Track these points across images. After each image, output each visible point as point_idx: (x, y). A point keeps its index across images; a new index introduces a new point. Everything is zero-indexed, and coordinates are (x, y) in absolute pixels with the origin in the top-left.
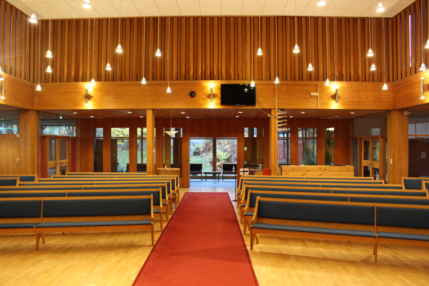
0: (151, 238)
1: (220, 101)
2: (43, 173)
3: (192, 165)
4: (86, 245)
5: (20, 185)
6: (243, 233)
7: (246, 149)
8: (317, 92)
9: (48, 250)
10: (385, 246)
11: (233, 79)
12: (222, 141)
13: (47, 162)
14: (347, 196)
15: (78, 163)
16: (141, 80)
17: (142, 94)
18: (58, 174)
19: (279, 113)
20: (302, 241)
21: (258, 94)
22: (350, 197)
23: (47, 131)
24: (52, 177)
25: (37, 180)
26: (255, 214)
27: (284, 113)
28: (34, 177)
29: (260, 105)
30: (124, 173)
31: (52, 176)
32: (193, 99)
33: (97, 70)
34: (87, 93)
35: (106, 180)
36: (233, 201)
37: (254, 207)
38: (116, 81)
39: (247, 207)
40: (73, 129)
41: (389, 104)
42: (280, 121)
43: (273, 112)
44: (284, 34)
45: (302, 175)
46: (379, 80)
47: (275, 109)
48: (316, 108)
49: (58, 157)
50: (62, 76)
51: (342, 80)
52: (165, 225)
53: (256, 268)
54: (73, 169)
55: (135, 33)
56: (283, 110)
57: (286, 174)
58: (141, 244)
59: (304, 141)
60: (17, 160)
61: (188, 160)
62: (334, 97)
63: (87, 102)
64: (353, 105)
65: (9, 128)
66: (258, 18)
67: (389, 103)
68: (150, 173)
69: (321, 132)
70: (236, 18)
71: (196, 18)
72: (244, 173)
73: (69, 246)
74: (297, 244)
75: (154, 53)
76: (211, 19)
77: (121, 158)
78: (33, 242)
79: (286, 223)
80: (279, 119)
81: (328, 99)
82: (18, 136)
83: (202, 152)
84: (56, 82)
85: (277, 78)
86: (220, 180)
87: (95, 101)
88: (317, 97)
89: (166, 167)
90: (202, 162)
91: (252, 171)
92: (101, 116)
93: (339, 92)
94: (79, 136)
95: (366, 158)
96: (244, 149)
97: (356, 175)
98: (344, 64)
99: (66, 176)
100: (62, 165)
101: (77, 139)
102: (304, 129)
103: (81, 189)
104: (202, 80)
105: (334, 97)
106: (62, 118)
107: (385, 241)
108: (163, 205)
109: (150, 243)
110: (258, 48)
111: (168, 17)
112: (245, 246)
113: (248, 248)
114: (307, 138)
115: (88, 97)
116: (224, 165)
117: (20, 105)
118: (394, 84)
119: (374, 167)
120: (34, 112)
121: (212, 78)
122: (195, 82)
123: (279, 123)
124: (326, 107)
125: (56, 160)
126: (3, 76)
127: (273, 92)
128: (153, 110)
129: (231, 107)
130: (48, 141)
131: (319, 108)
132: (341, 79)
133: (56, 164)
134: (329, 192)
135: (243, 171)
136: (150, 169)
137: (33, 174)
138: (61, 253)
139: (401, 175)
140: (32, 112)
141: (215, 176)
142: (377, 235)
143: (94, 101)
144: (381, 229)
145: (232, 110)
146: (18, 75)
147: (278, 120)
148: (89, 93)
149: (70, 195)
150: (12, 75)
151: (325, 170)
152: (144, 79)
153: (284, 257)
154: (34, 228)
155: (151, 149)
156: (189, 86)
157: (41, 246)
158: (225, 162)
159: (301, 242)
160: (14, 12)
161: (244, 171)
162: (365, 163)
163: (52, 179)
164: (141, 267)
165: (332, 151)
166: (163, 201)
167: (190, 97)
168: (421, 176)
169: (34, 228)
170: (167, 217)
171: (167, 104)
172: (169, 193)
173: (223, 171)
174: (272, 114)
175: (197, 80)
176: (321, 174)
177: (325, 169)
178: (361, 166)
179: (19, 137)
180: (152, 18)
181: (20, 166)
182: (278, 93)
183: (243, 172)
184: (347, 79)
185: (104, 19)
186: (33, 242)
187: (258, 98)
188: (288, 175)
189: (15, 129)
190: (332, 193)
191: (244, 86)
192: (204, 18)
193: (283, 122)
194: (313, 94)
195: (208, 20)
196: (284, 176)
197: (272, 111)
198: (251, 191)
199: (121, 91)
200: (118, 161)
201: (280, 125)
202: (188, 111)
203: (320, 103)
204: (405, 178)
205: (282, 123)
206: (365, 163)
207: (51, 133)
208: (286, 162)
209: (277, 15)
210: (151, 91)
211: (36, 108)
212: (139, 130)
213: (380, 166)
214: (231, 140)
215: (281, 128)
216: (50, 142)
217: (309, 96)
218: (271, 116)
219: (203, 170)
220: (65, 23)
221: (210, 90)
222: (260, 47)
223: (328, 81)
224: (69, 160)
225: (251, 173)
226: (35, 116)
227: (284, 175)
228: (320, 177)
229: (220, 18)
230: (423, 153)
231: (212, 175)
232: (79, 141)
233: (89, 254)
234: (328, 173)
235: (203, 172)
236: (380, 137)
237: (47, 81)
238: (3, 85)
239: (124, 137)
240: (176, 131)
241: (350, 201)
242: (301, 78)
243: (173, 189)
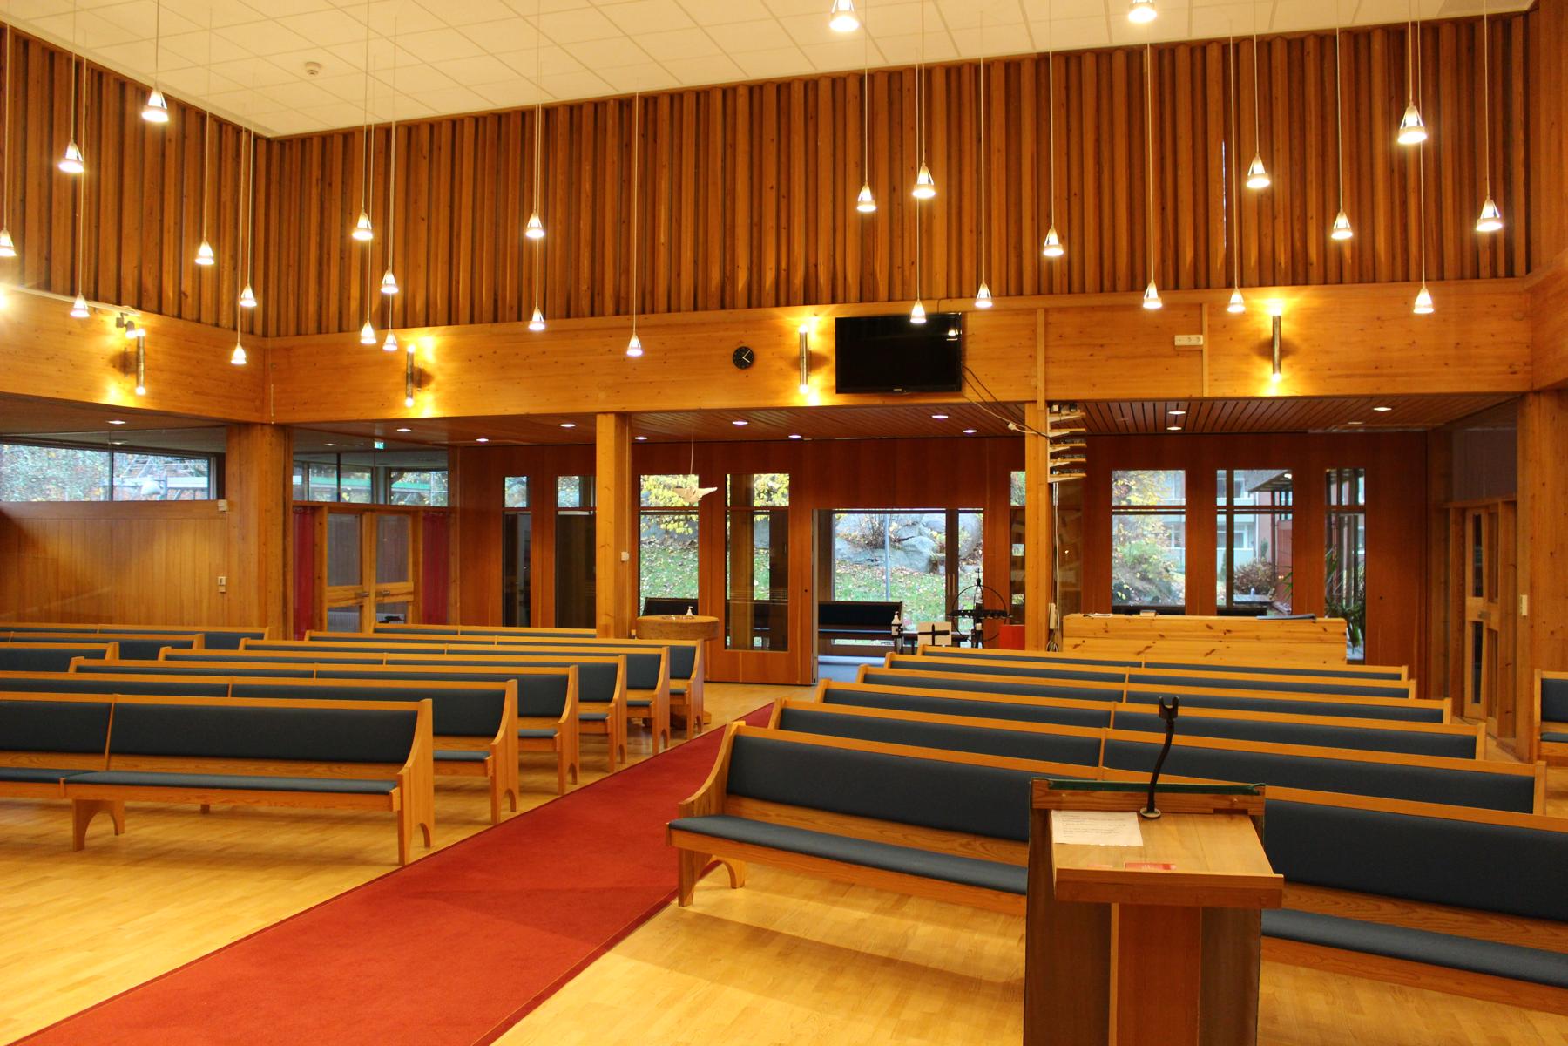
1: (833, 382)
8: (1201, 332)
11: (886, 299)
13: (321, 589)
15: (454, 594)
16: (974, 295)
17: (582, 364)
19: (1056, 418)
27: (1077, 414)
32: (742, 374)
34: (412, 366)
35: (442, 652)
41: (1511, 370)
42: (1060, 448)
45: (1139, 653)
46: (1468, 272)
51: (1306, 283)
55: (561, 156)
57: (1076, 646)
60: (219, 583)
63: (411, 396)
64: (1347, 376)
66: (977, 68)
67: (1510, 367)
68: (606, 633)
76: (810, 86)
77: (675, 578)
79: (807, 820)
80: (1055, 441)
81: (1247, 356)
85: (984, 291)
87: (437, 390)
88: (1201, 351)
94: (458, 505)
98: (1312, 218)
101: (453, 515)
103: (309, 675)
104: (777, 304)
106: (385, 445)
110: (862, 185)
114: (1290, 513)
115: (418, 378)
118: (1526, 287)
120: (268, 430)
122: (756, 313)
123: (1054, 456)
124: (1235, 391)
125: (361, 583)
127: (1030, 339)
133: (362, 596)
135: (930, 630)
136: (608, 618)
140: (262, 429)
143: (437, 390)
145: (1213, 404)
147: (1051, 443)
149: (240, 692)
150: (166, 315)
151: (1228, 634)
152: (537, 315)
154: (62, 783)
156: (728, 329)
167: (735, 368)
169: (62, 783)
171: (659, 393)
174: (1026, 424)
175: (760, 306)
176: (1213, 651)
177: (1229, 631)
178: (1463, 622)
179: (225, 508)
180: (615, 100)
181: (229, 600)
182: (1046, 342)
183: (930, 636)
184: (653, 309)
185: (443, 120)
190: (234, 695)
193: (1073, 451)
194: (1182, 340)
199: (517, 354)
201: (1060, 462)
203: (1211, 374)
204: (1551, 675)
205: (1067, 456)
209: (869, 67)
210: (610, 351)
211: (272, 416)
215: (1063, 473)
218: (1024, 429)
221: (1270, 325)
222: (867, 183)
224: (415, 585)
226: (271, 444)
227: (1070, 648)
232: (458, 520)
236: (1500, 504)
238: (142, 352)
240: (702, 485)
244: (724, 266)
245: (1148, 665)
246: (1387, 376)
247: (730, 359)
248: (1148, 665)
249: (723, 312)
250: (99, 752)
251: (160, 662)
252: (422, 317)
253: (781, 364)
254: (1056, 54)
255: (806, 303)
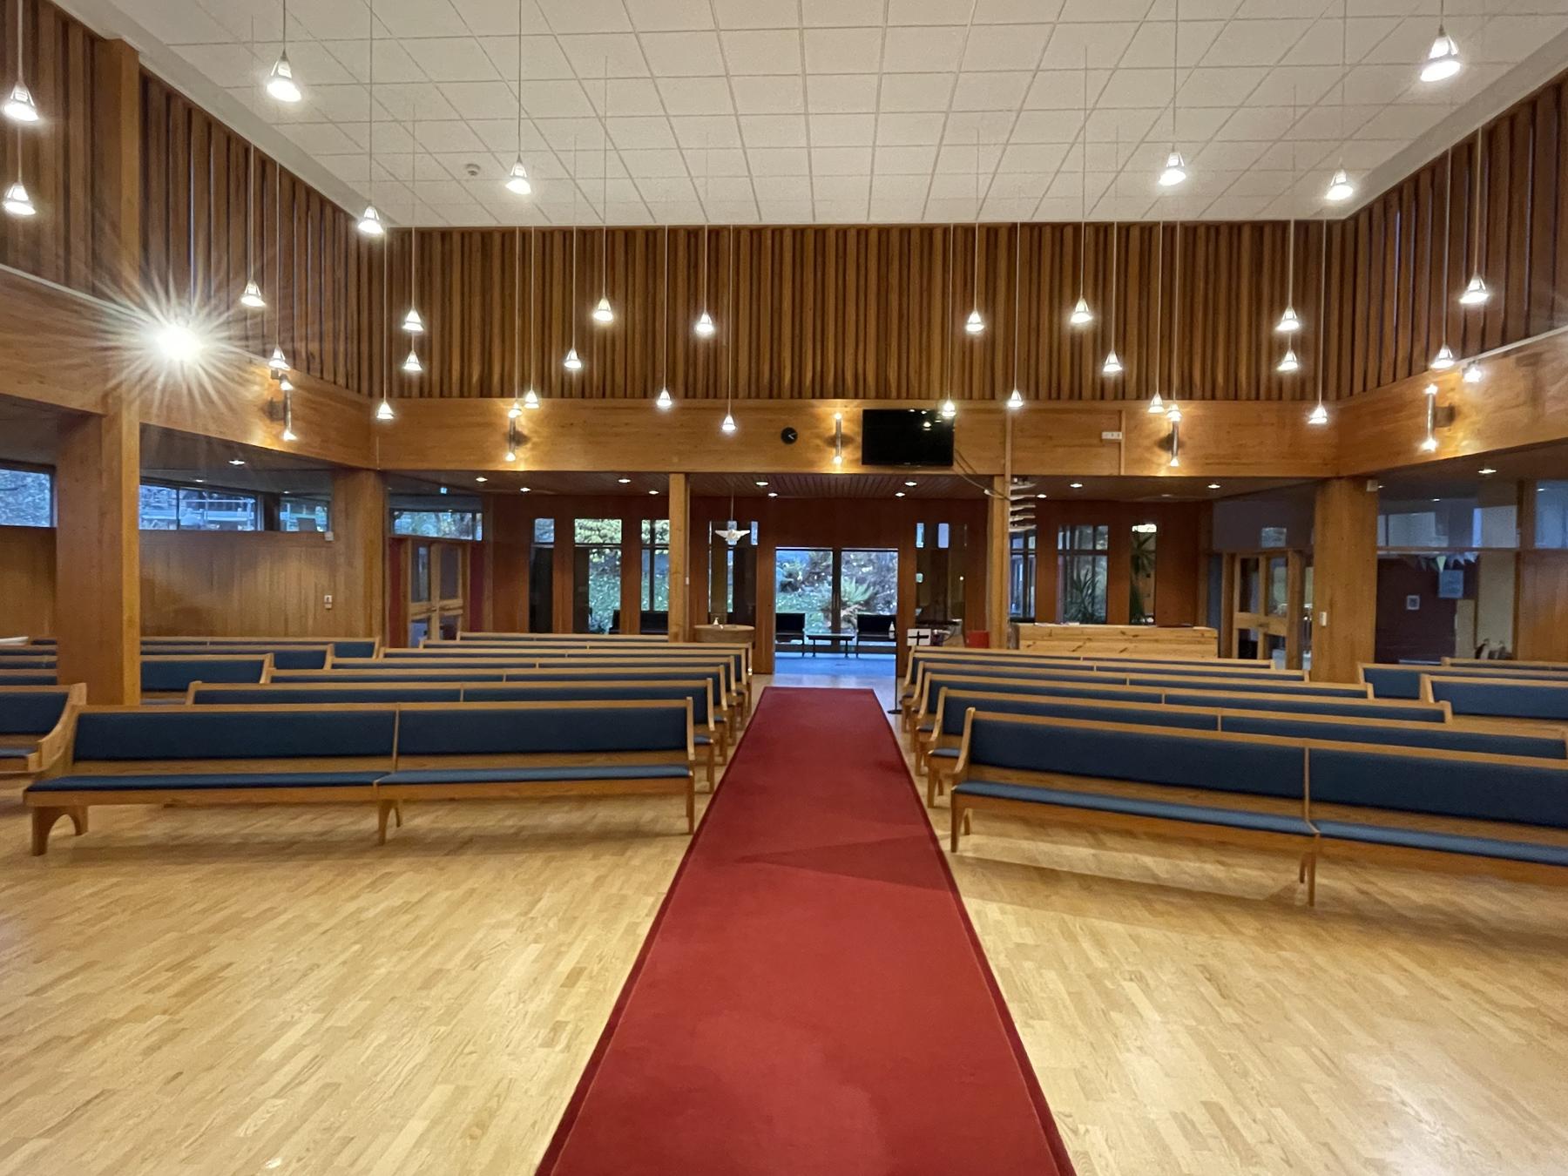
0: (684, 812)
1: (859, 454)
2: (397, 637)
3: (779, 616)
4: (512, 831)
5: (334, 666)
6: (924, 801)
7: (919, 577)
8: (1120, 430)
9: (412, 845)
10: (1333, 860)
12: (852, 556)
13: (406, 607)
14: (1214, 714)
16: (655, 394)
18: (436, 637)
20: (1088, 832)
21: (958, 437)
22: (1222, 717)
23: (405, 524)
24: (421, 646)
25: (381, 655)
26: (963, 755)
27: (1028, 485)
28: (372, 645)
29: (964, 466)
30: (606, 636)
31: (423, 640)
33: (540, 365)
36: (889, 712)
37: (961, 734)
38: (591, 397)
39: (935, 734)
40: (474, 518)
43: (997, 482)
44: (1035, 275)
47: (1003, 475)
48: (1115, 473)
49: (436, 592)
50: (446, 381)
51: (1191, 398)
52: (719, 775)
53: (971, 905)
54: (476, 625)
56: (1024, 478)
57: (1029, 646)
58: (659, 827)
59: (1068, 558)
61: (771, 603)
62: (1167, 443)
65: (304, 515)
68: (676, 638)
69: (1121, 540)
70: (905, 231)
71: (799, 232)
72: (919, 640)
73: (468, 833)
74: (1078, 841)
75: (688, 325)
78: (371, 822)
80: (1014, 503)
82: (329, 536)
83: (803, 583)
84: (430, 396)
86: (849, 655)
88: (1120, 444)
89: (716, 623)
90: (803, 609)
91: (937, 636)
92: (548, 490)
93: (1181, 429)
95: (1244, 608)
96: (915, 578)
97: (1224, 652)
99: (458, 642)
100: (447, 614)
102: (1068, 527)
103: (499, 678)
105: (1167, 443)
107: (1341, 849)
108: (716, 722)
109: (683, 825)
111: (726, 228)
112: (934, 839)
113: (946, 846)
115: (517, 439)
116: (860, 618)
117: (337, 455)
119: (1272, 632)
121: (839, 394)
122: (797, 402)
123: (1013, 513)
125: (429, 599)
126: (289, 377)
128: (687, 475)
129: (888, 471)
130: (410, 551)
131: (1123, 473)
132: (1187, 396)
134: (1156, 699)
137: (370, 635)
138: (447, 855)
139: (1353, 659)
141: (835, 645)
142: (1316, 831)
144: (1323, 811)
146: (328, 376)
148: (519, 429)
153: (1047, 876)
154: (375, 786)
155: (680, 576)
157: (391, 833)
158: (859, 610)
159: (1087, 835)
160: (315, 207)
161: (919, 637)
162: (1241, 620)
163: (421, 650)
164: (664, 896)
165: (1148, 585)
166: (715, 713)
167: (781, 443)
168: (1405, 658)
169: (375, 786)
170: (723, 754)
172: (728, 689)
173: (858, 633)
175: (800, 397)
179: (331, 539)
186: (371, 822)
187: (959, 447)
188: (1034, 650)
189: (320, 515)
191: (918, 417)
192: (821, 232)
194: (1107, 435)
195: (831, 236)
196: (1022, 651)
197: (996, 480)
198: (946, 693)
200: (592, 604)
201: (1017, 518)
202: (775, 479)
206: (1241, 620)
207: (414, 530)
208: (1020, 611)
212: (645, 525)
213: (1290, 630)
214: (874, 554)
216: (416, 555)
217: (1095, 441)
219: (807, 631)
220: (451, 238)
223: (1157, 399)
225: (937, 641)
228: (1125, 656)
229: (863, 231)
230: (1414, 597)
231: (828, 643)
233: (519, 858)
234: (1144, 646)
235: (806, 633)
237: (406, 394)
238: (289, 402)
239: (604, 544)
241: (1223, 730)
242: (1076, 394)
243: (738, 679)
244: (1183, 372)
245: (1085, 659)
246: (1244, 464)
247: (779, 435)
248: (1085, 659)
249: (771, 401)
250: (387, 754)
251: (327, 670)
252: (832, 394)
253: (818, 442)
254: (1023, 225)
255: (836, 397)
